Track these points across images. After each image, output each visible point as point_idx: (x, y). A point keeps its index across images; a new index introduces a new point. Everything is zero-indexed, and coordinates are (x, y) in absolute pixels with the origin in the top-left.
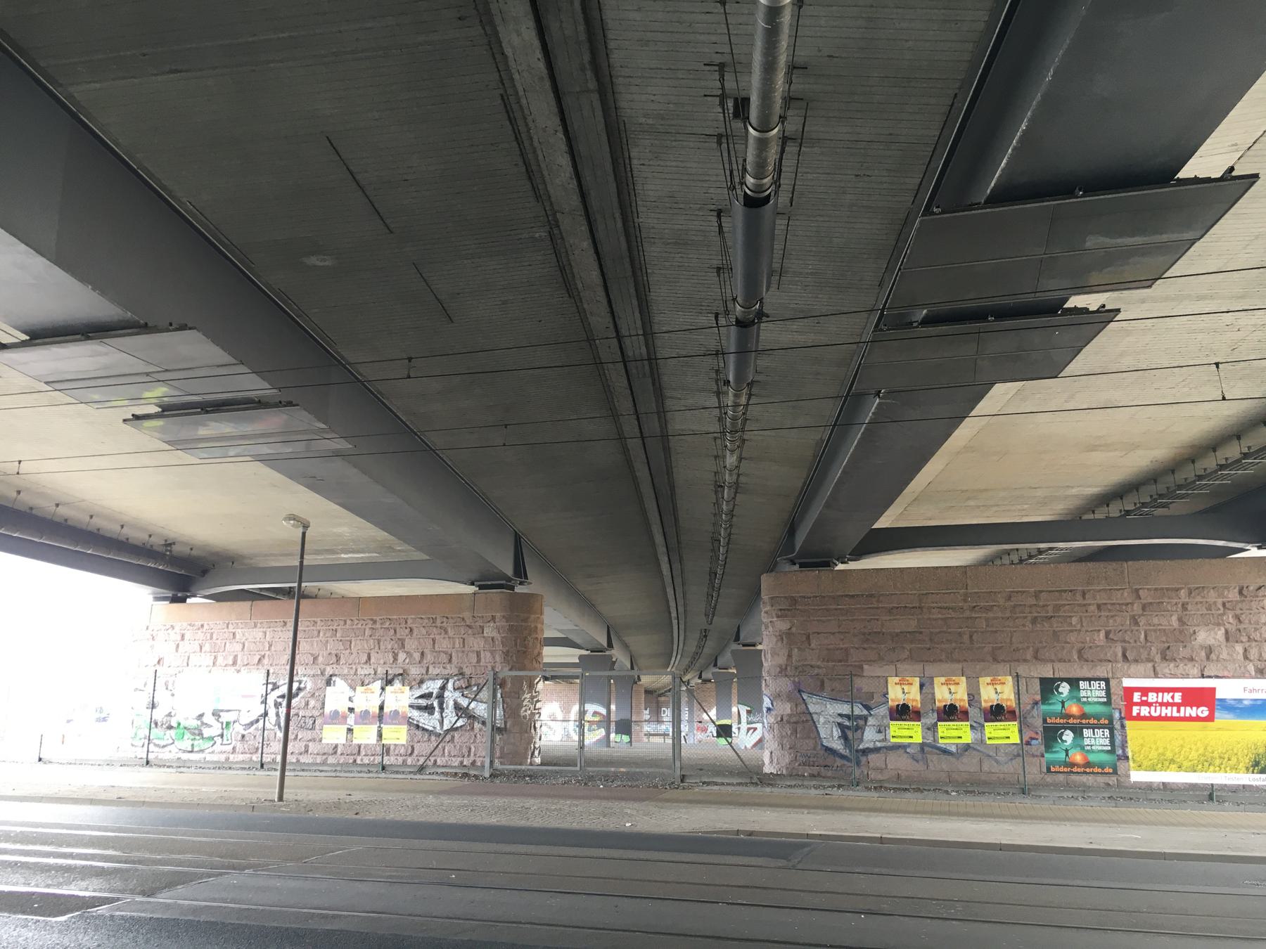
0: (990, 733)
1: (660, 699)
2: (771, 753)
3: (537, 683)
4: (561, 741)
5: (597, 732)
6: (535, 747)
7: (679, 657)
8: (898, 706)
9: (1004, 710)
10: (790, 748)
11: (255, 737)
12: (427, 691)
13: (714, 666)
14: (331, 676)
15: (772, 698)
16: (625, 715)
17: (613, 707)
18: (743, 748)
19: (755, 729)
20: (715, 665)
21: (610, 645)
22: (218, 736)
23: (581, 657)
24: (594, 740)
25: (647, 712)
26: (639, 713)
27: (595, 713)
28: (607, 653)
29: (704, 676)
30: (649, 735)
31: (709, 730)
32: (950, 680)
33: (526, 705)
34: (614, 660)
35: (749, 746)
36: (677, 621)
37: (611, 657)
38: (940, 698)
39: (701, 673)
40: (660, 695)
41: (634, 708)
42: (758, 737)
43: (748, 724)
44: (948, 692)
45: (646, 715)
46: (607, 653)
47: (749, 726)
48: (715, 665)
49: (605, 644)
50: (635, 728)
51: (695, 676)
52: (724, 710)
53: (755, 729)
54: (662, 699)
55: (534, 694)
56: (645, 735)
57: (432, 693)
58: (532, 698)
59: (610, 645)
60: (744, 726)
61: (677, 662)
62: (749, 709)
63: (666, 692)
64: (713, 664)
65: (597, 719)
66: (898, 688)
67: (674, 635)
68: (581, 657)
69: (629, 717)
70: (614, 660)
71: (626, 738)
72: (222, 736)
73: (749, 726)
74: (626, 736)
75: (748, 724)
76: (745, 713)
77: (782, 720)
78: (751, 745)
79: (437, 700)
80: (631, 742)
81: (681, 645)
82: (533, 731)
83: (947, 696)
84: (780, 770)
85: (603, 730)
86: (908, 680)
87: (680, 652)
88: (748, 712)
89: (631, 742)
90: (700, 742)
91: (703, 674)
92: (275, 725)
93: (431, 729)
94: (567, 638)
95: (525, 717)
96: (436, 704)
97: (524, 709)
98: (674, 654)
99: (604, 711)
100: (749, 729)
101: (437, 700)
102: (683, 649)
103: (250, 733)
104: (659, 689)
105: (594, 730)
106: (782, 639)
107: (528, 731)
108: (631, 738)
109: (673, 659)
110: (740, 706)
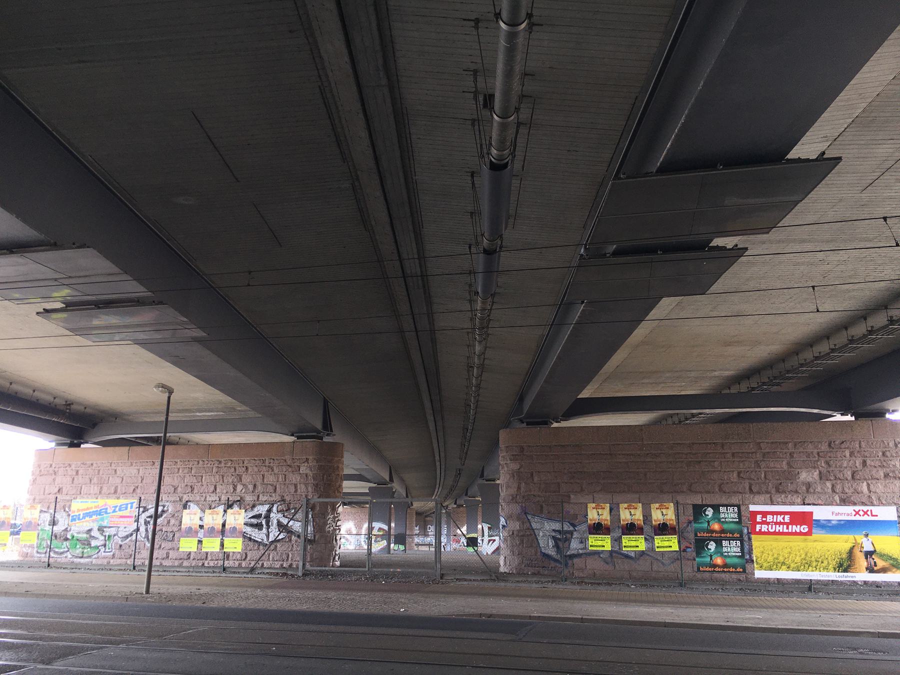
0: (659, 543)
1: (264, 567)
2: (505, 558)
3: (338, 507)
6: (336, 554)
8: (594, 523)
9: (602, 527)
11: (129, 546)
12: (258, 513)
13: (465, 495)
14: (187, 502)
16: (401, 530)
17: (393, 525)
18: (485, 554)
19: (494, 540)
20: (466, 495)
21: (391, 480)
22: (102, 546)
23: (370, 488)
24: (379, 548)
25: (418, 528)
26: (412, 529)
27: (380, 529)
30: (418, 545)
31: (461, 541)
32: (630, 505)
33: (330, 523)
34: (394, 490)
35: (489, 553)
38: (591, 518)
40: (426, 516)
43: (489, 537)
44: (211, 519)
45: (417, 530)
47: (490, 538)
48: (466, 495)
50: (408, 540)
52: (472, 528)
53: (494, 540)
56: (416, 545)
57: (262, 514)
58: (335, 517)
59: (391, 480)
60: (486, 538)
61: (439, 493)
62: (490, 526)
64: (464, 494)
65: (381, 533)
66: (659, 512)
68: (370, 488)
69: (403, 532)
70: (394, 490)
71: (402, 547)
72: (105, 545)
73: (490, 538)
75: (489, 537)
77: (513, 534)
79: (265, 520)
80: (405, 550)
81: (442, 480)
82: (334, 542)
83: (660, 517)
85: (385, 541)
86: (665, 506)
89: (405, 550)
91: (457, 500)
92: (145, 538)
93: (260, 540)
95: (329, 532)
96: (264, 523)
97: (328, 526)
98: (438, 486)
99: (386, 527)
100: (489, 541)
101: (265, 520)
103: (126, 544)
107: (331, 542)
108: (405, 547)
109: (437, 490)
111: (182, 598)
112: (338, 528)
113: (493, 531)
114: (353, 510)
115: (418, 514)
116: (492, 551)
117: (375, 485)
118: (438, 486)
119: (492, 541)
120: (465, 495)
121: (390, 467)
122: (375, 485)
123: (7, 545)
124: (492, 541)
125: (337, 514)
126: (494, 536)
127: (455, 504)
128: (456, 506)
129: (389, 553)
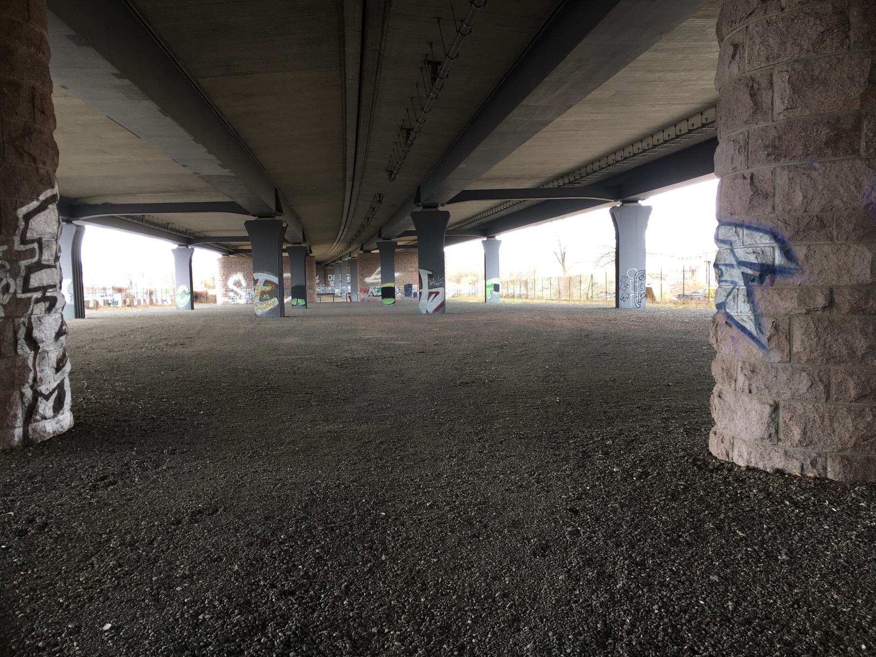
2: (775, 408)
3: (28, 217)
4: (247, 303)
5: (270, 302)
6: (37, 394)
7: (346, 230)
10: (860, 397)
13: (378, 237)
15: (786, 234)
16: (299, 282)
17: (287, 275)
18: (425, 313)
19: (437, 293)
20: (380, 236)
21: (279, 209)
24: (267, 309)
25: (317, 278)
26: (312, 279)
27: (267, 282)
28: (277, 218)
29: (365, 248)
30: (319, 295)
35: (431, 310)
36: (351, 183)
37: (281, 222)
39: (362, 245)
40: (327, 265)
41: (307, 275)
42: (440, 302)
43: (429, 289)
46: (277, 218)
48: (380, 236)
49: (273, 207)
50: (309, 292)
51: (356, 249)
52: (387, 275)
53: (437, 293)
54: (329, 268)
55: (18, 247)
56: (318, 294)
59: (279, 209)
60: (426, 290)
61: (343, 237)
62: (431, 273)
63: (331, 262)
64: (377, 235)
65: (268, 288)
67: (346, 205)
68: (248, 224)
70: (284, 225)
71: (301, 302)
74: (301, 300)
75: (429, 289)
76: (426, 277)
77: (831, 304)
78: (433, 310)
80: (306, 304)
81: (351, 215)
82: (24, 349)
84: (814, 464)
85: (276, 299)
87: (348, 224)
88: (430, 276)
89: (306, 304)
90: (363, 300)
91: (364, 246)
94: (234, 202)
98: (342, 227)
99: (275, 280)
100: (430, 294)
102: (351, 221)
104: (327, 261)
105: (267, 300)
106: (845, 24)
108: (306, 302)
109: (340, 233)
110: (421, 271)
111: (207, 309)
112: (38, 295)
113: (436, 279)
114: (242, 260)
115: (318, 263)
116: (435, 307)
117: (253, 218)
118: (342, 227)
119: (434, 295)
120: (378, 237)
121: (276, 191)
122: (253, 218)
123: (153, 289)
124: (434, 295)
125: (24, 241)
126: (436, 287)
127: (362, 249)
128: (362, 252)
129: (282, 314)
